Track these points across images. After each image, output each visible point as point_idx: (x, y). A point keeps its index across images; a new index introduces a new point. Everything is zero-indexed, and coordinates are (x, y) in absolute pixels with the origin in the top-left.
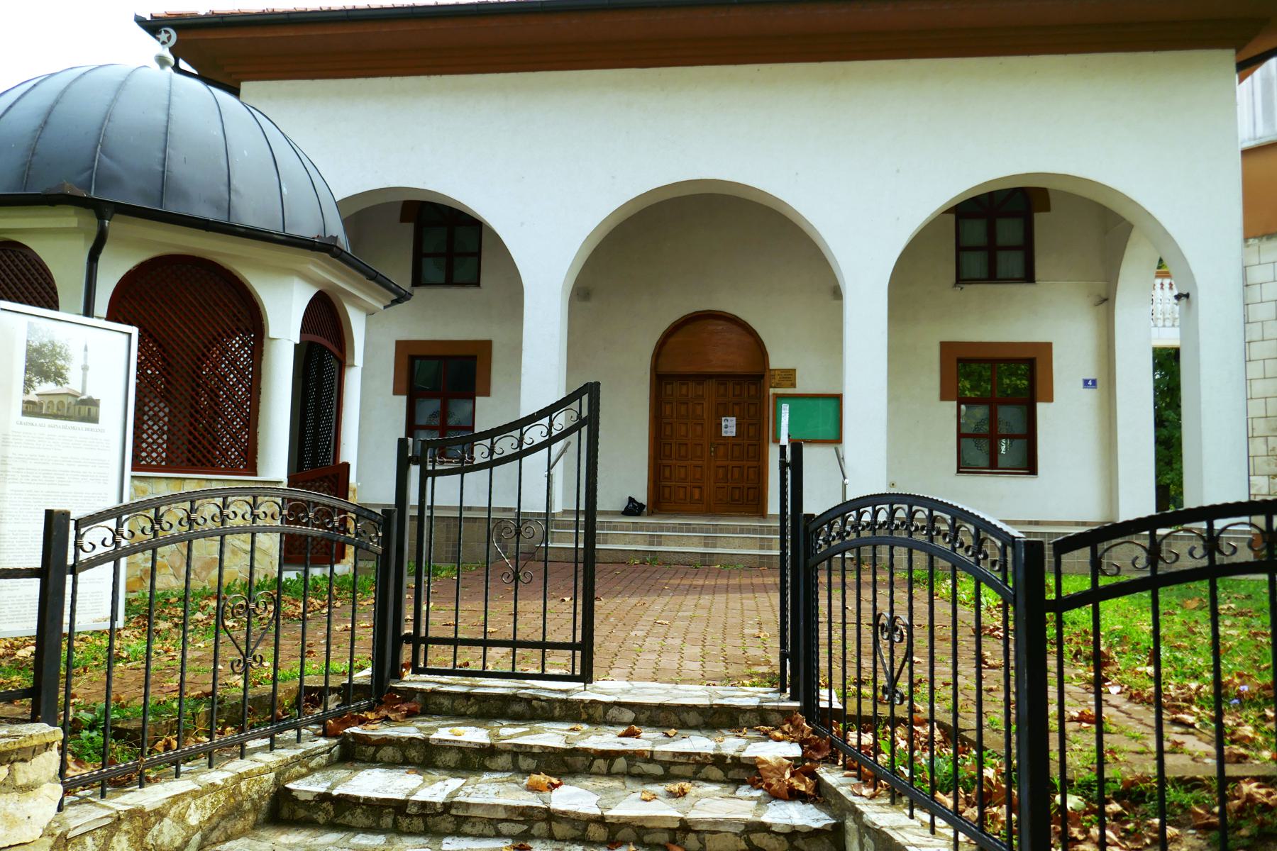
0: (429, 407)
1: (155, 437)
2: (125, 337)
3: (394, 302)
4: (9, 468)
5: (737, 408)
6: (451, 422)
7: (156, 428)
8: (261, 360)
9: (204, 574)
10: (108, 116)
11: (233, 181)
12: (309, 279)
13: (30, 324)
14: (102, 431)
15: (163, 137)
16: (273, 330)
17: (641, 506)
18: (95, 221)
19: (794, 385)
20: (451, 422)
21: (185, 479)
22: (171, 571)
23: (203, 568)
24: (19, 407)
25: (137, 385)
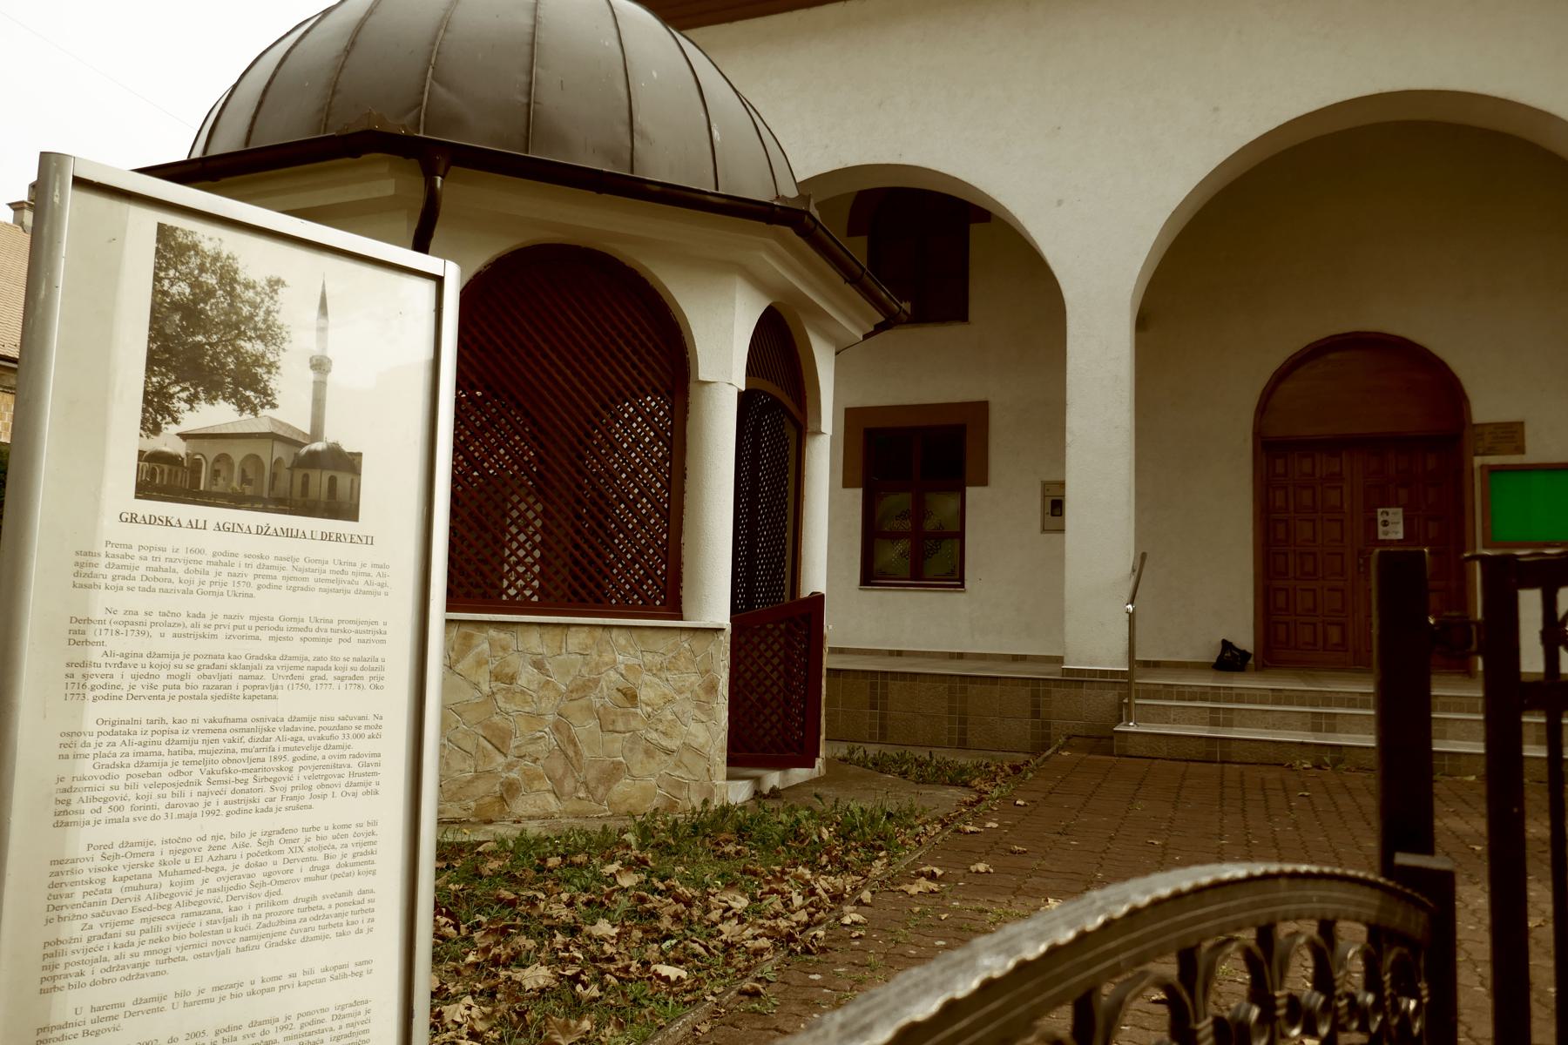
0: (897, 501)
1: (521, 553)
2: (429, 287)
3: (879, 328)
4: (95, 654)
5: (1403, 494)
6: (929, 525)
7: (522, 538)
8: (684, 419)
9: (601, 790)
10: (445, 23)
11: (638, 118)
12: (758, 282)
13: (163, 232)
14: (369, 541)
15: (526, 49)
16: (705, 368)
17: (1245, 655)
18: (419, 183)
19: (1521, 450)
20: (929, 525)
21: (568, 625)
22: (548, 785)
23: (599, 781)
24: (123, 472)
25: (458, 402)
